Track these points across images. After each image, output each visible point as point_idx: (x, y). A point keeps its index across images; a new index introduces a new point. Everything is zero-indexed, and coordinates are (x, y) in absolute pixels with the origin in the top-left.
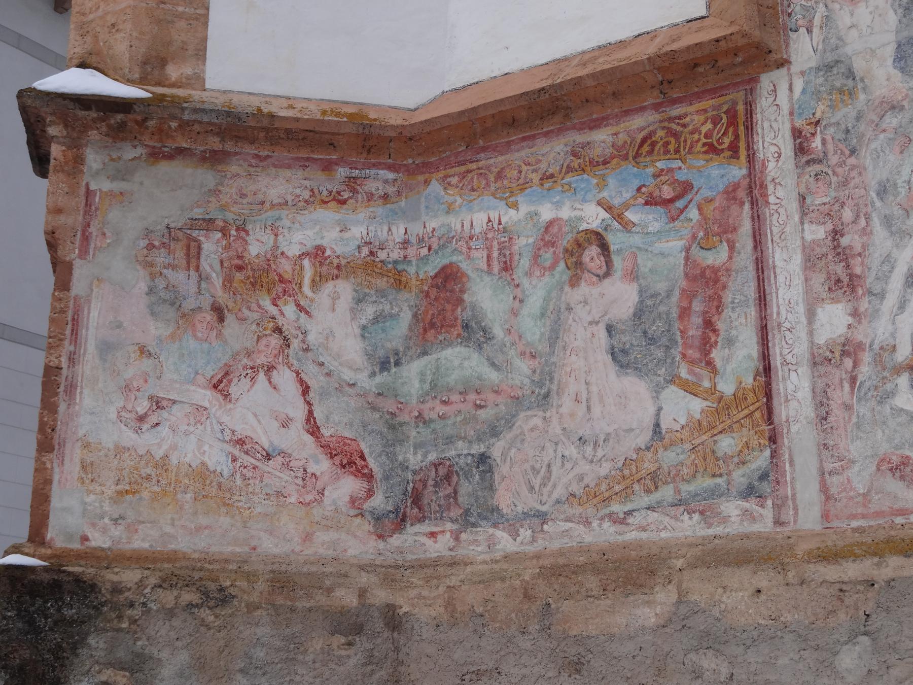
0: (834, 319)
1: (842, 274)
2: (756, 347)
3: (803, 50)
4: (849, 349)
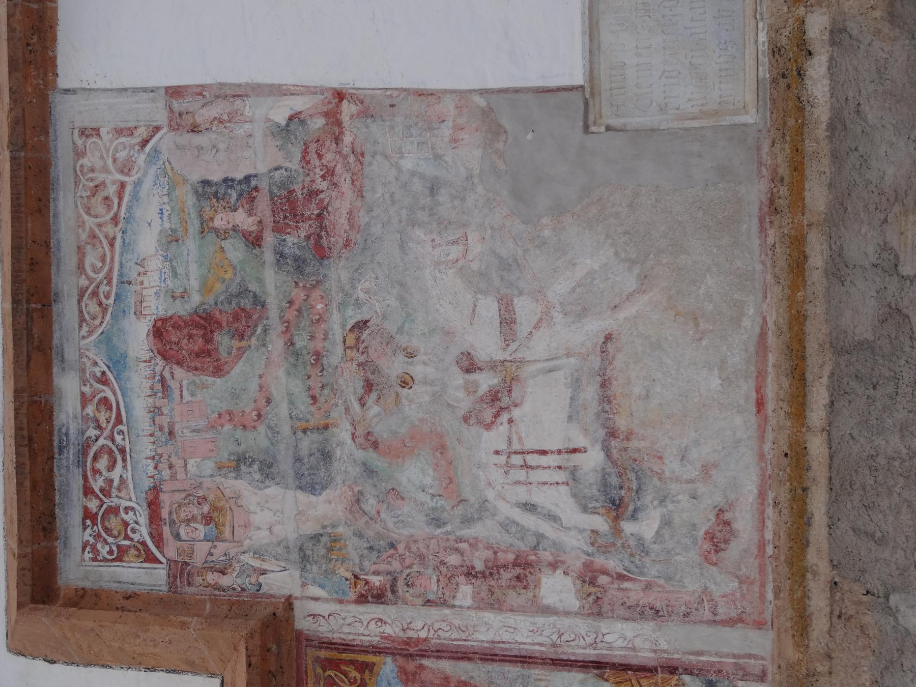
0: (557, 588)
1: (511, 573)
2: (742, 423)
3: (281, 581)
4: (589, 577)
